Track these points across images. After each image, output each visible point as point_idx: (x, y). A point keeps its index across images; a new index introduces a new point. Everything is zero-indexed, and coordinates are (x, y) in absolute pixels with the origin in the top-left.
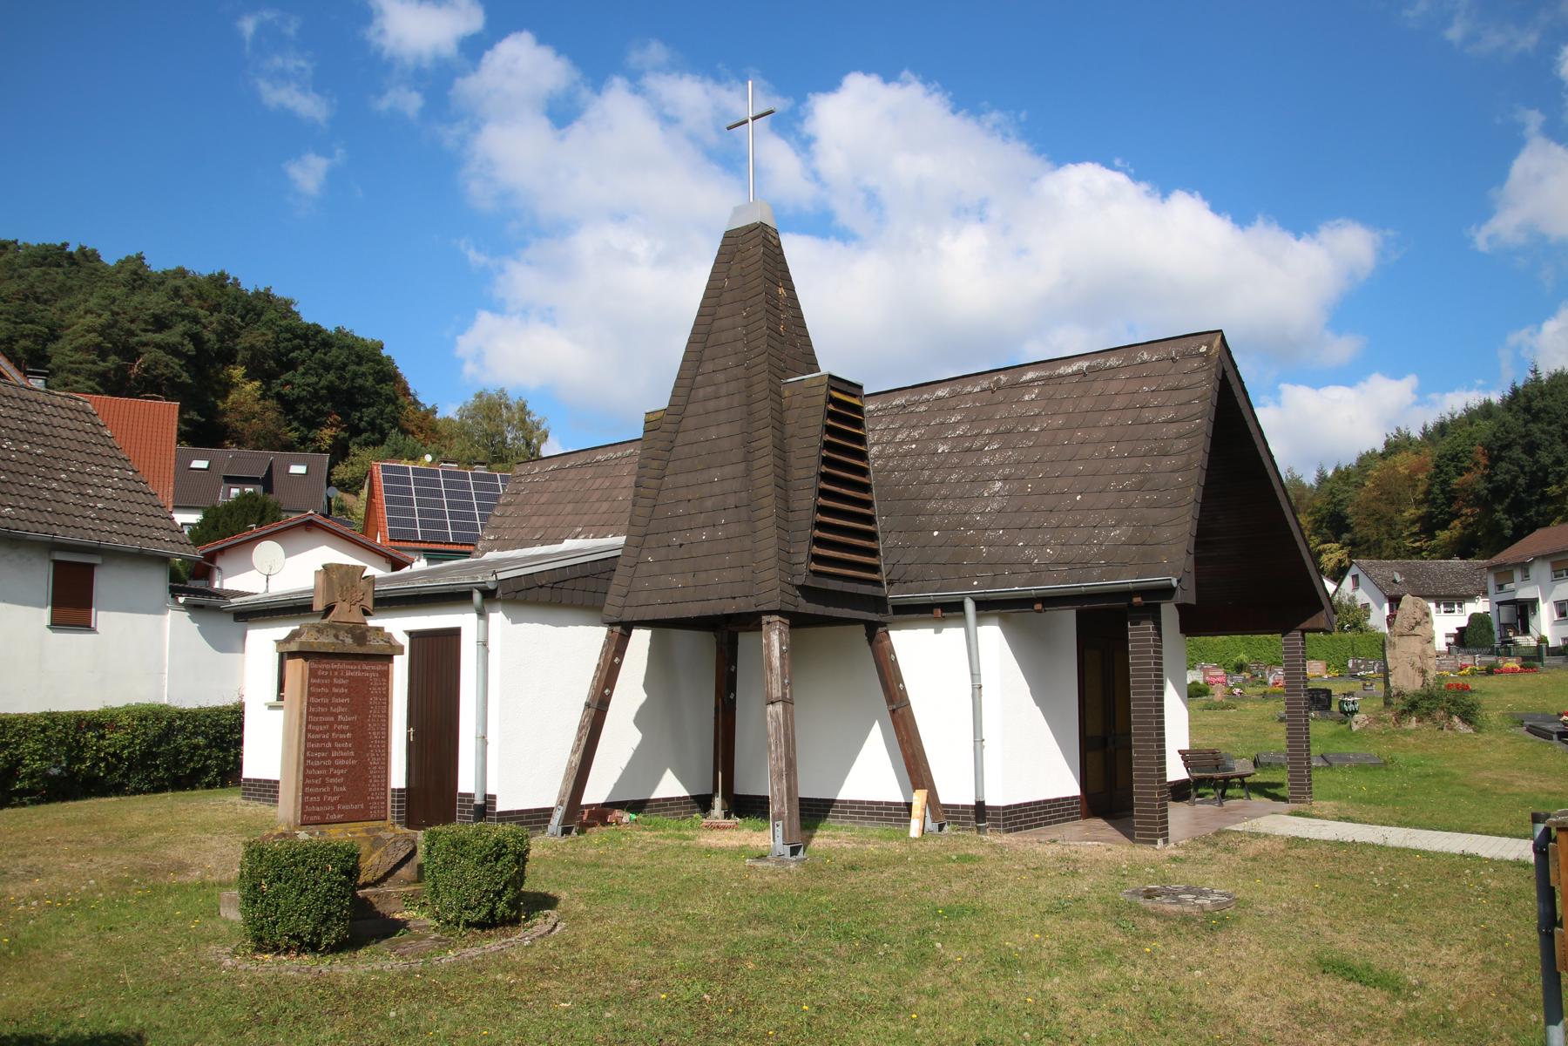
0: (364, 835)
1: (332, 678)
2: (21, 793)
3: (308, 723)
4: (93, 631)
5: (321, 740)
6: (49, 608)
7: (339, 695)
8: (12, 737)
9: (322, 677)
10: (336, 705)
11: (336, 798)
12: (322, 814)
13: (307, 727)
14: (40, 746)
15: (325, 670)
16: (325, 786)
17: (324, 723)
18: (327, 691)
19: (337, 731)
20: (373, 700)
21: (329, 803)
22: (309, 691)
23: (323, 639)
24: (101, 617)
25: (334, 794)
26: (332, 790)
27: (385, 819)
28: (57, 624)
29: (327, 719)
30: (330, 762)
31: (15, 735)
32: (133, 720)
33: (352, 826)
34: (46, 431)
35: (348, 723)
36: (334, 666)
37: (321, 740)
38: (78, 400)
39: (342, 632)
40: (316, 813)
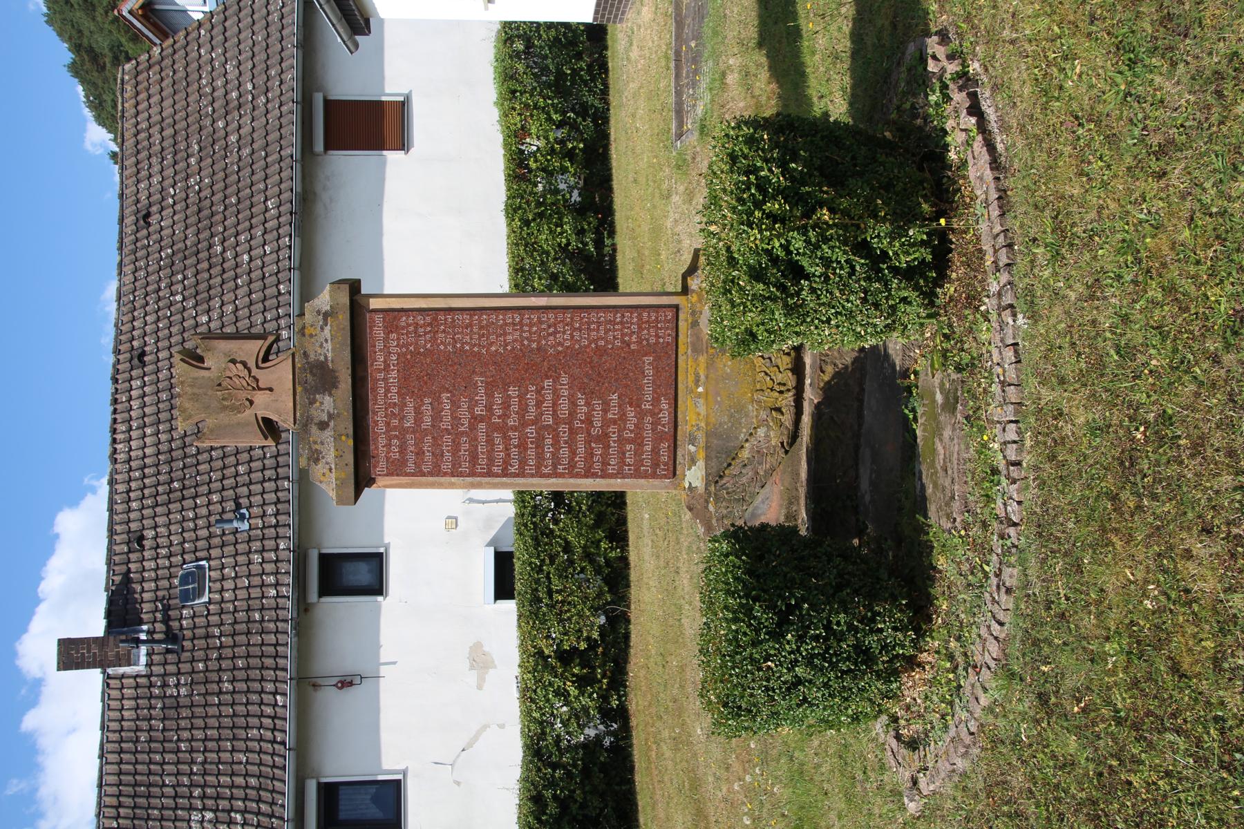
0: (702, 359)
1: (404, 431)
2: (599, 243)
3: (489, 474)
4: (408, 98)
5: (522, 446)
6: (385, 152)
7: (437, 417)
8: (535, 260)
9: (403, 450)
10: (456, 419)
11: (631, 413)
12: (659, 438)
13: (497, 476)
14: (546, 227)
15: (389, 445)
16: (606, 435)
17: (490, 441)
18: (429, 439)
19: (505, 416)
20: (444, 342)
21: (639, 427)
22: (431, 474)
23: (330, 455)
24: (392, 90)
25: (623, 417)
26: (614, 422)
27: (677, 307)
28: (402, 143)
29: (482, 437)
30: (563, 428)
31: (532, 256)
32: (514, 109)
33: (685, 381)
34: (169, 132)
35: (490, 395)
36: (382, 428)
37: (522, 446)
38: (122, 80)
39: (313, 412)
40: (655, 451)
